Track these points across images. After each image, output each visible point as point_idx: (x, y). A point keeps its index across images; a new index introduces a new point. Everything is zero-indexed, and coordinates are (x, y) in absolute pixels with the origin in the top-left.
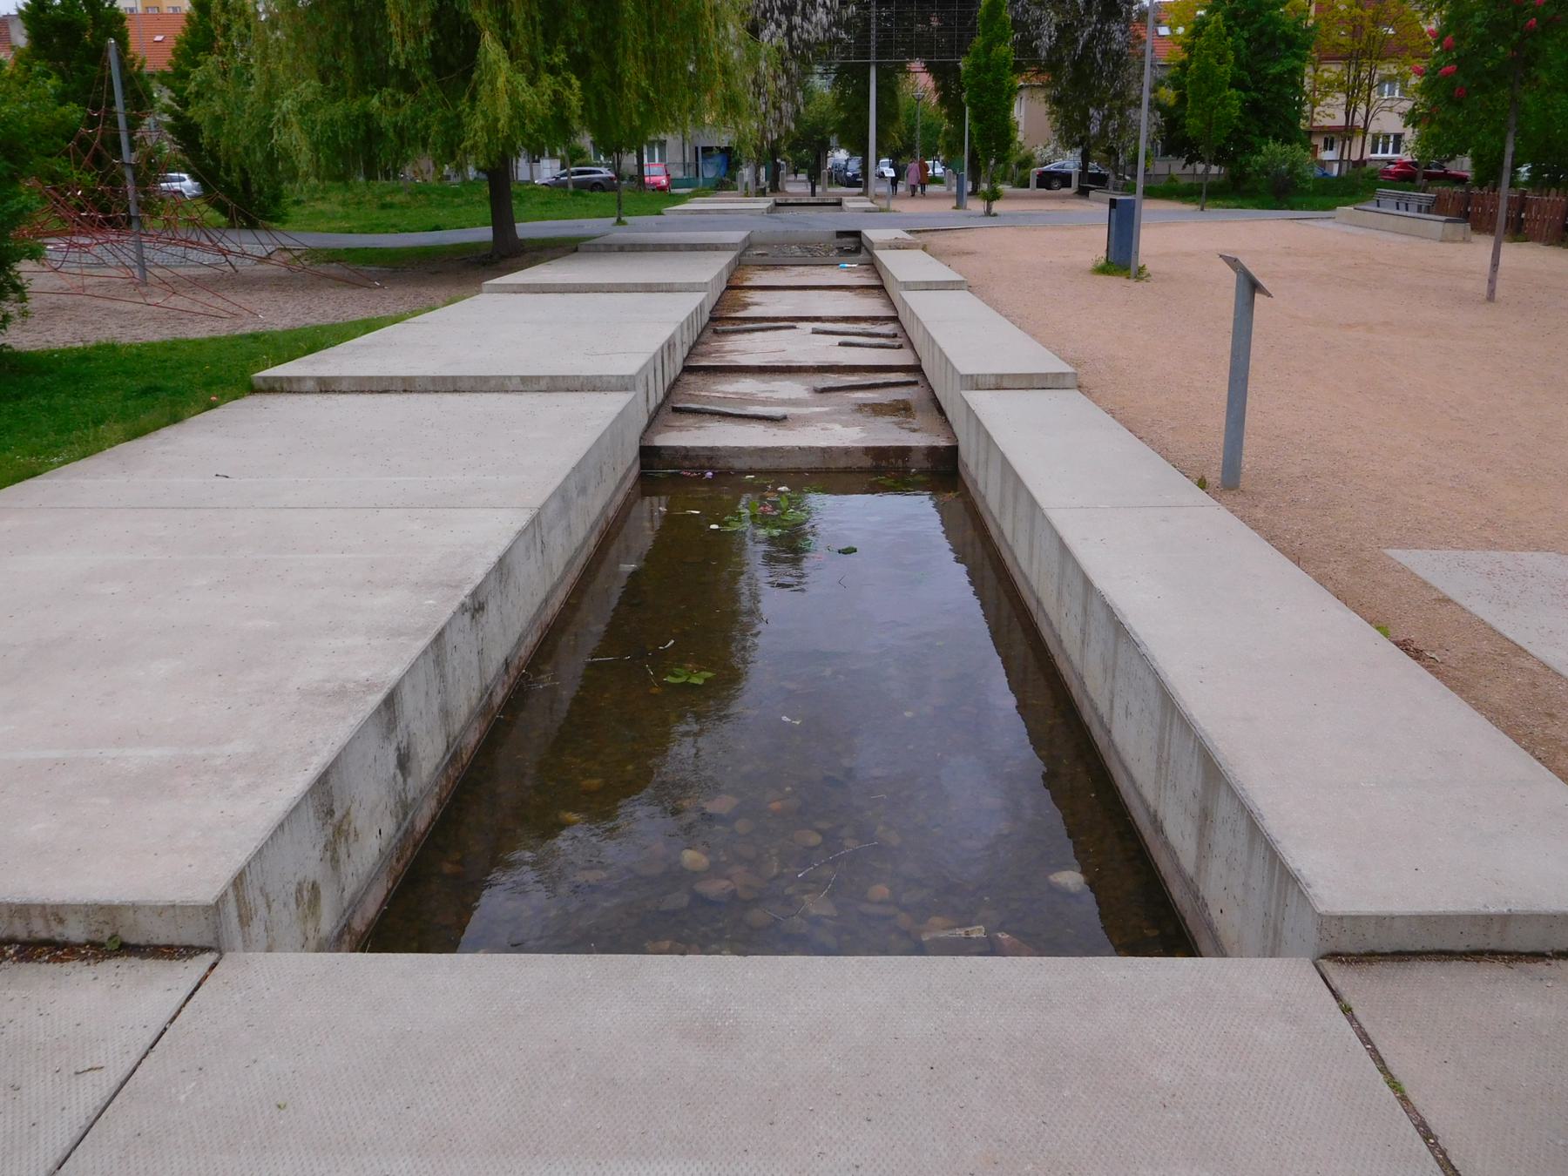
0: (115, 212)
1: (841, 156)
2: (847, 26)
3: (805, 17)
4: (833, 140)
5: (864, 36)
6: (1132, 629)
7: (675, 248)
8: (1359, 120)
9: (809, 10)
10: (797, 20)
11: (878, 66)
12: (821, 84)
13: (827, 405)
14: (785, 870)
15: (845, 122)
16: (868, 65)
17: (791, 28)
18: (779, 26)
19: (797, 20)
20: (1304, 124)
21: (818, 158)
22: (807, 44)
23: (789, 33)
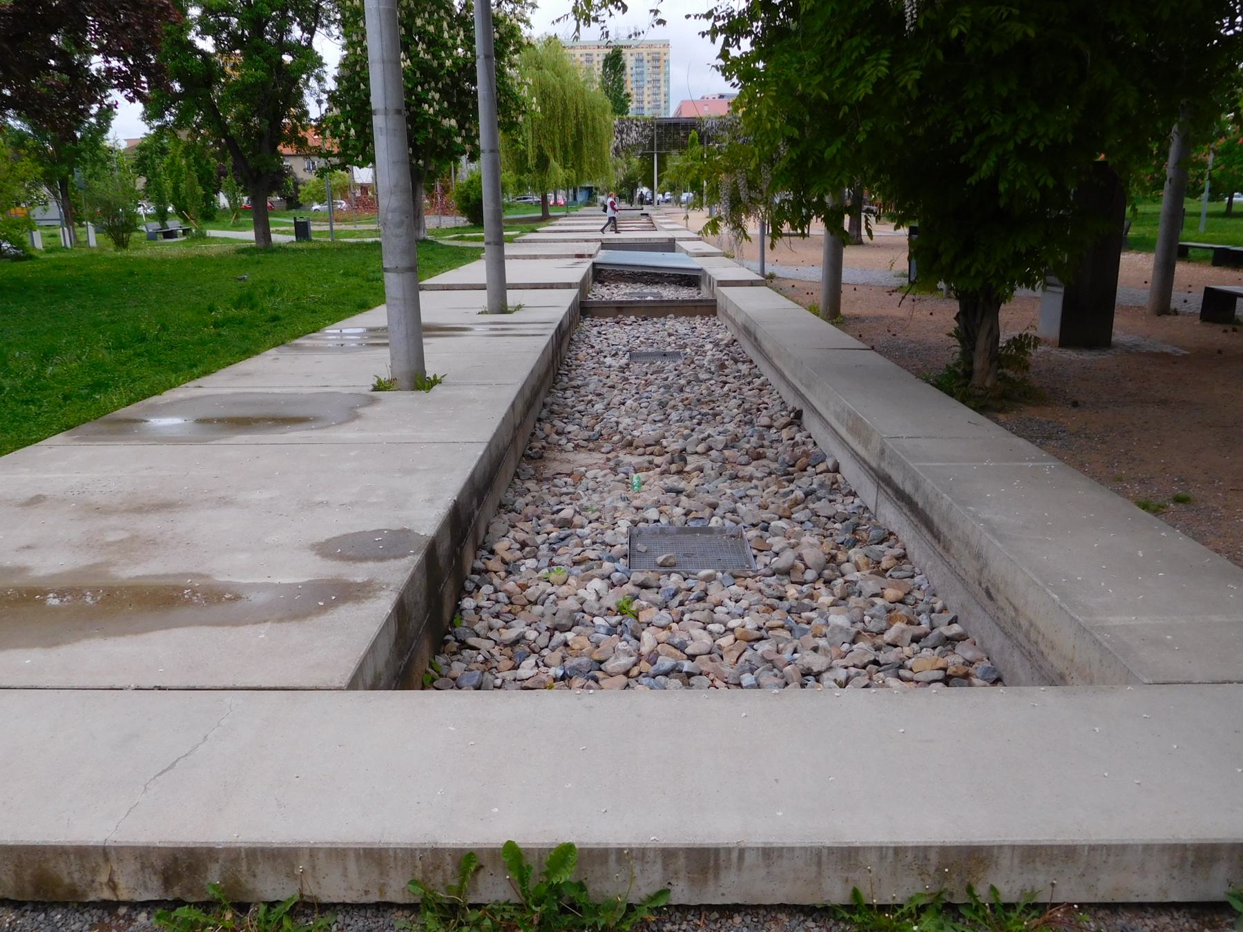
0: (196, 132)
1: (645, 190)
2: (647, 136)
3: (627, 134)
4: (640, 184)
5: (652, 141)
6: (848, 856)
7: (586, 216)
8: (806, 232)
9: (629, 131)
10: (624, 136)
11: (658, 154)
12: (635, 161)
13: (342, 243)
14: (72, 857)
15: (644, 176)
16: (653, 154)
17: (622, 139)
18: (617, 138)
19: (624, 136)
20: (885, 178)
21: (632, 192)
22: (629, 145)
23: (621, 141)
